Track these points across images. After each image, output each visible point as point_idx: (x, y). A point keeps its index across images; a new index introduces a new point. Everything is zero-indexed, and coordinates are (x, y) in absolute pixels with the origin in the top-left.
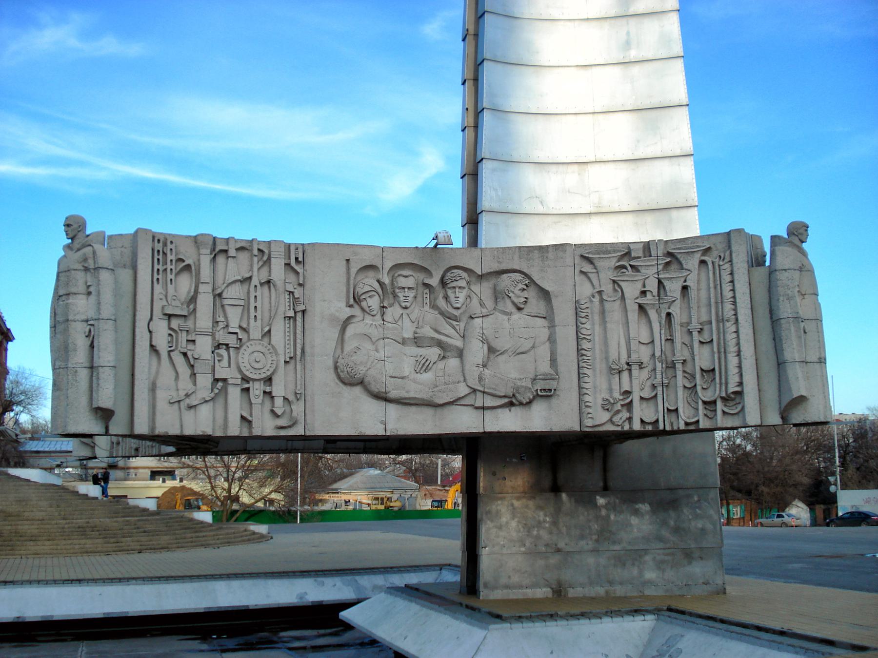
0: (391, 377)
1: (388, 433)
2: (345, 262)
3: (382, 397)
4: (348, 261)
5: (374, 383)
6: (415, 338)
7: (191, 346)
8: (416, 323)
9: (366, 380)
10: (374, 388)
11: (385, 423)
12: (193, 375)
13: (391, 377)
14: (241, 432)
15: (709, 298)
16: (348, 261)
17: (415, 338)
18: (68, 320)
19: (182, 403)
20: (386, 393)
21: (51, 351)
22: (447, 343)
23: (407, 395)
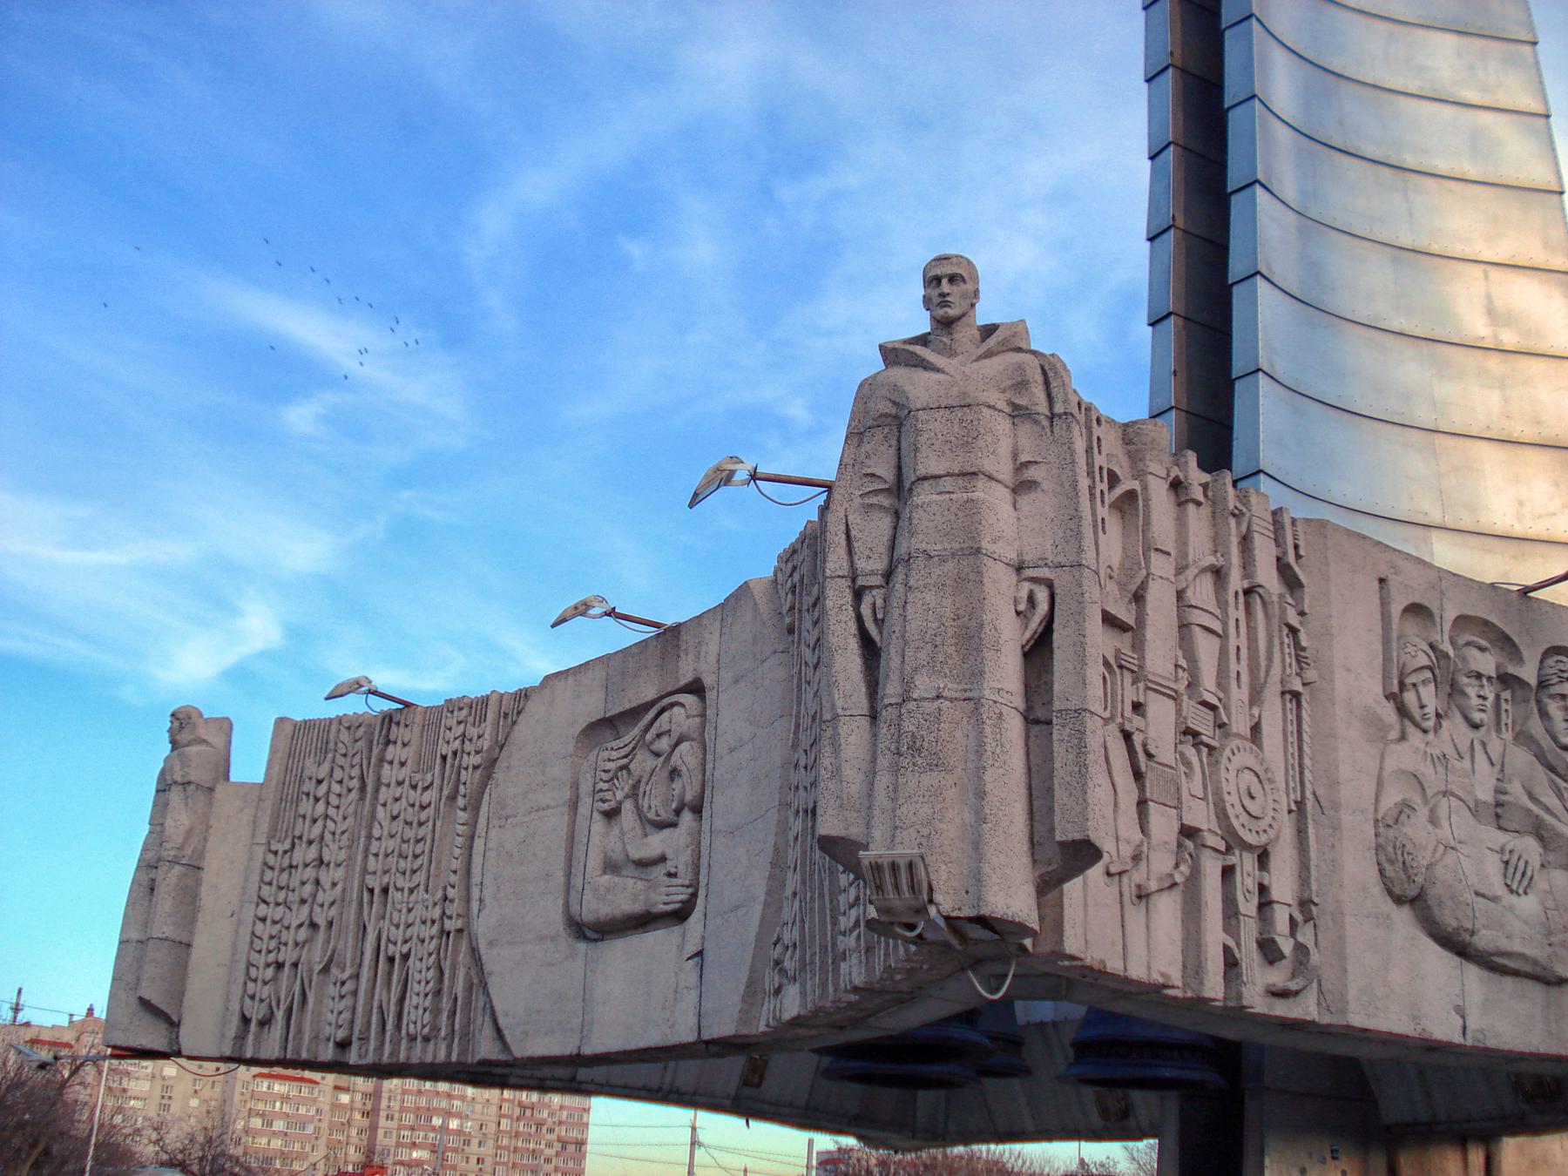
0: (1477, 894)
1: (1469, 1042)
2: (1376, 584)
3: (1457, 945)
4: (1381, 581)
5: (1449, 903)
6: (1499, 804)
7: (1138, 721)
8: (1498, 767)
9: (1433, 892)
10: (1448, 919)
11: (1460, 1011)
12: (1142, 804)
13: (1477, 894)
14: (742, 1021)
15: (369, 1022)
16: (1381, 581)
17: (1499, 804)
18: (979, 550)
19: (1125, 879)
20: (1473, 933)
21: (116, 979)
22: (1553, 829)
23: (1504, 944)
